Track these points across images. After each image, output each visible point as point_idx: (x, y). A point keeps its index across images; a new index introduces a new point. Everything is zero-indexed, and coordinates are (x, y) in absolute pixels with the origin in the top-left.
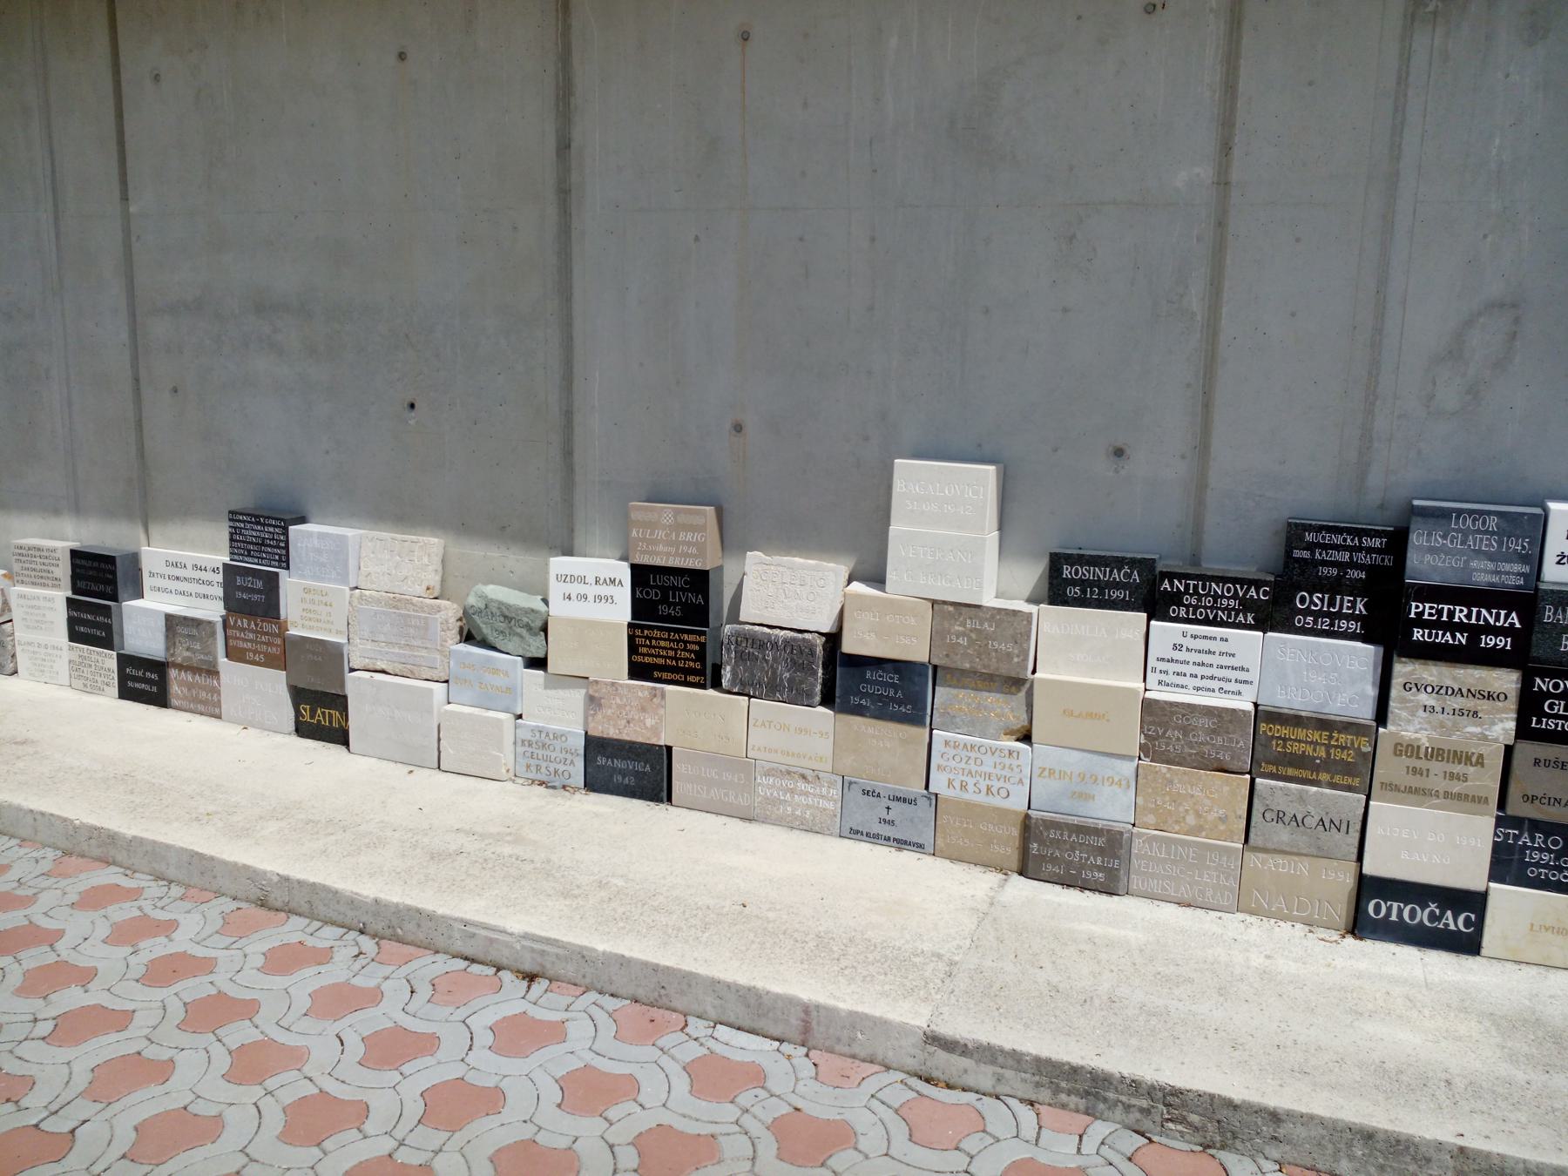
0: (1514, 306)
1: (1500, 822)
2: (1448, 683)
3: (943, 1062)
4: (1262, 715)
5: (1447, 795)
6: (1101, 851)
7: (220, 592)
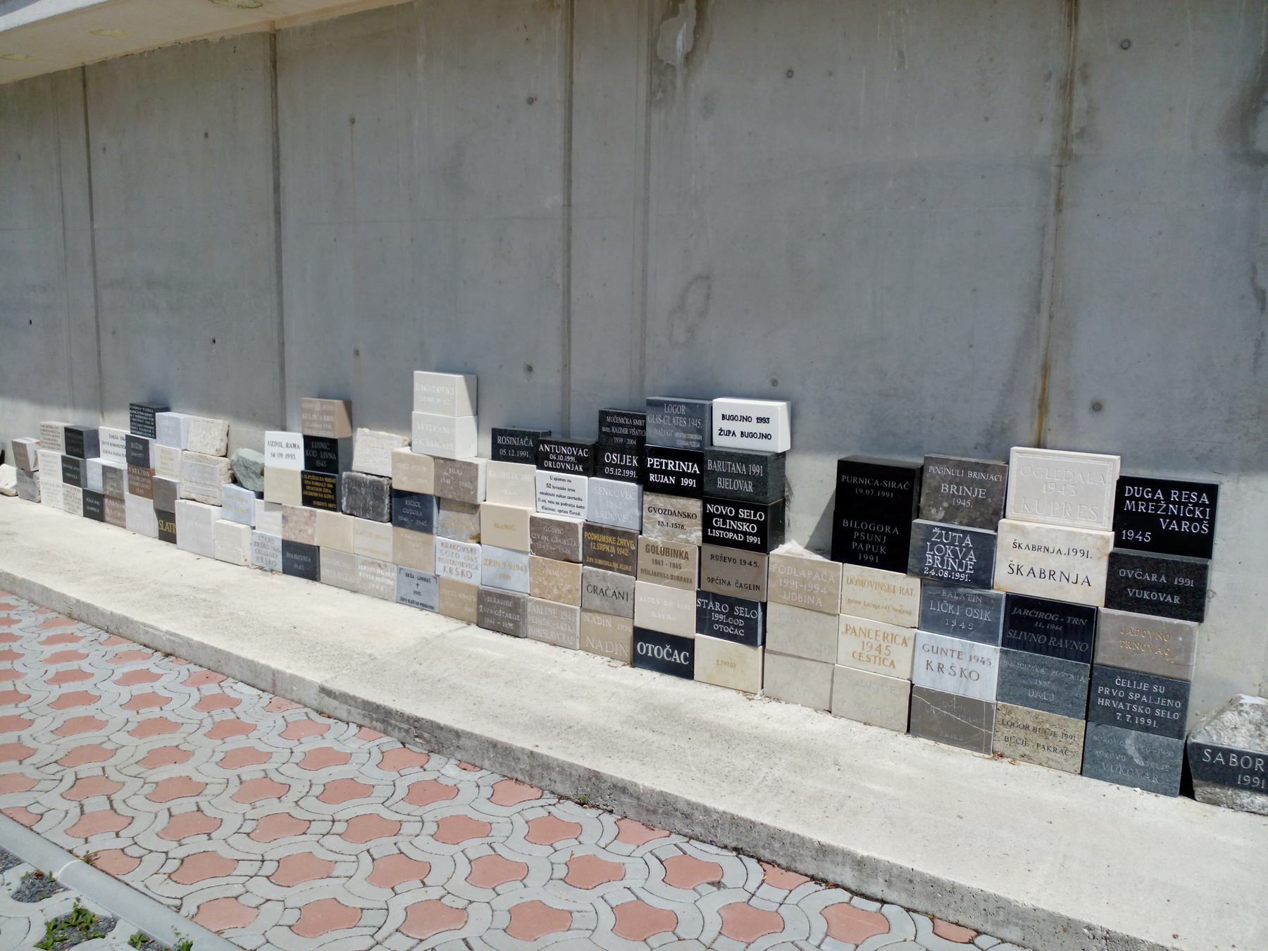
0: (708, 278)
1: (700, 594)
2: (669, 507)
3: (330, 704)
4: (588, 527)
5: (672, 577)
6: (511, 610)
7: (124, 451)
